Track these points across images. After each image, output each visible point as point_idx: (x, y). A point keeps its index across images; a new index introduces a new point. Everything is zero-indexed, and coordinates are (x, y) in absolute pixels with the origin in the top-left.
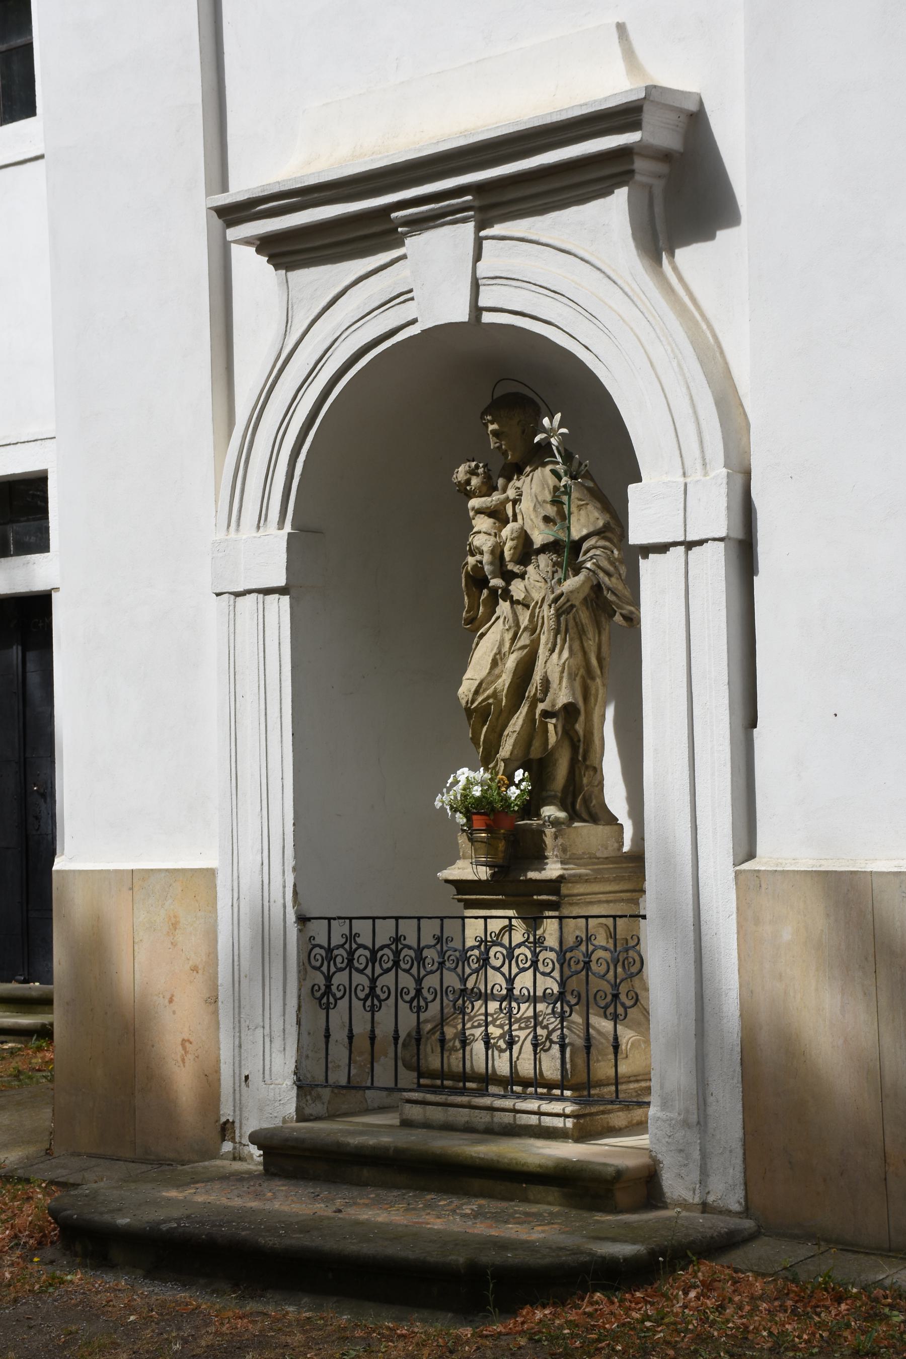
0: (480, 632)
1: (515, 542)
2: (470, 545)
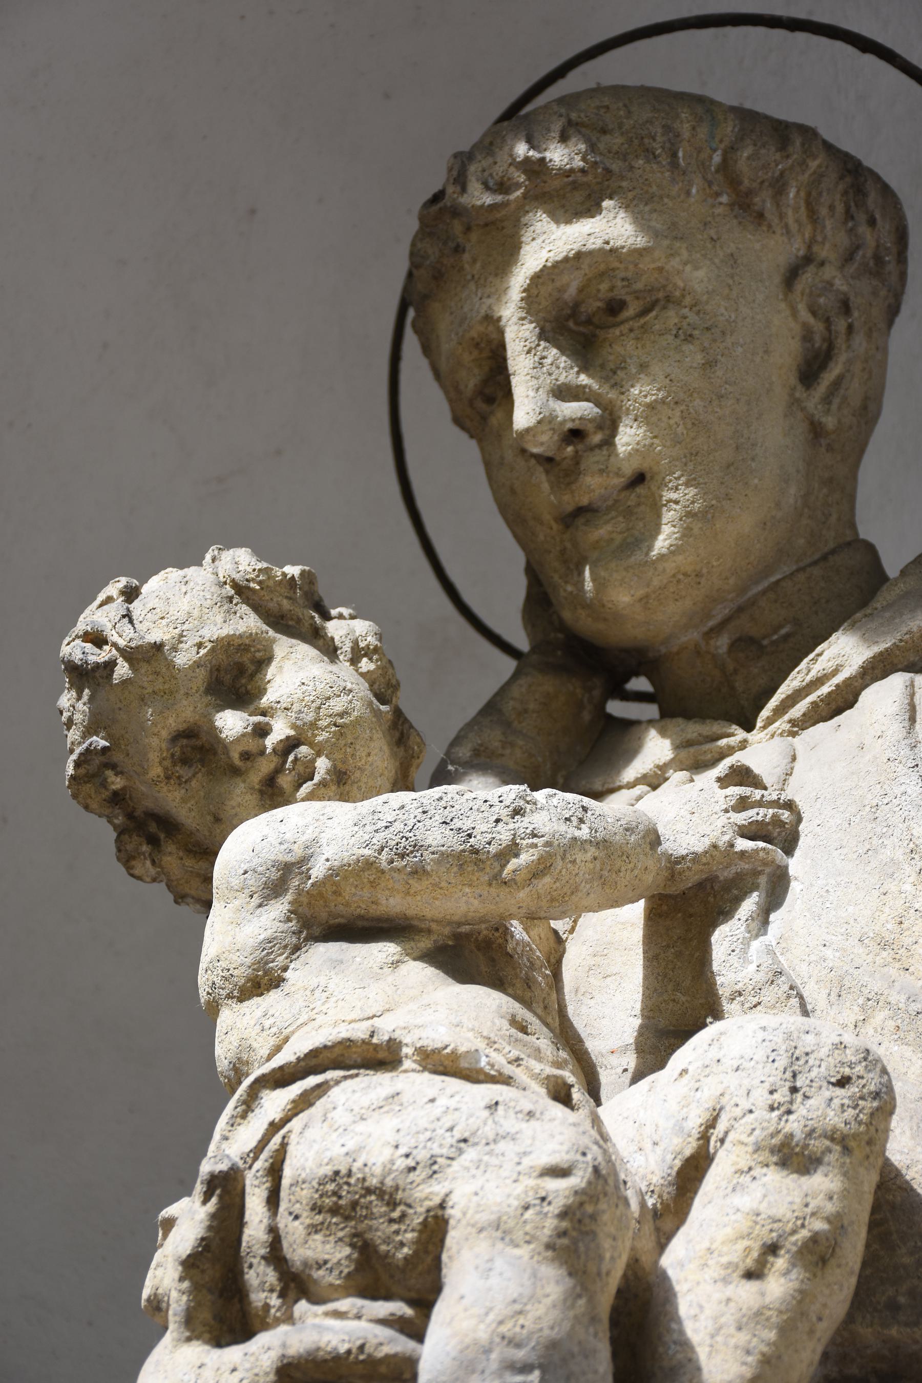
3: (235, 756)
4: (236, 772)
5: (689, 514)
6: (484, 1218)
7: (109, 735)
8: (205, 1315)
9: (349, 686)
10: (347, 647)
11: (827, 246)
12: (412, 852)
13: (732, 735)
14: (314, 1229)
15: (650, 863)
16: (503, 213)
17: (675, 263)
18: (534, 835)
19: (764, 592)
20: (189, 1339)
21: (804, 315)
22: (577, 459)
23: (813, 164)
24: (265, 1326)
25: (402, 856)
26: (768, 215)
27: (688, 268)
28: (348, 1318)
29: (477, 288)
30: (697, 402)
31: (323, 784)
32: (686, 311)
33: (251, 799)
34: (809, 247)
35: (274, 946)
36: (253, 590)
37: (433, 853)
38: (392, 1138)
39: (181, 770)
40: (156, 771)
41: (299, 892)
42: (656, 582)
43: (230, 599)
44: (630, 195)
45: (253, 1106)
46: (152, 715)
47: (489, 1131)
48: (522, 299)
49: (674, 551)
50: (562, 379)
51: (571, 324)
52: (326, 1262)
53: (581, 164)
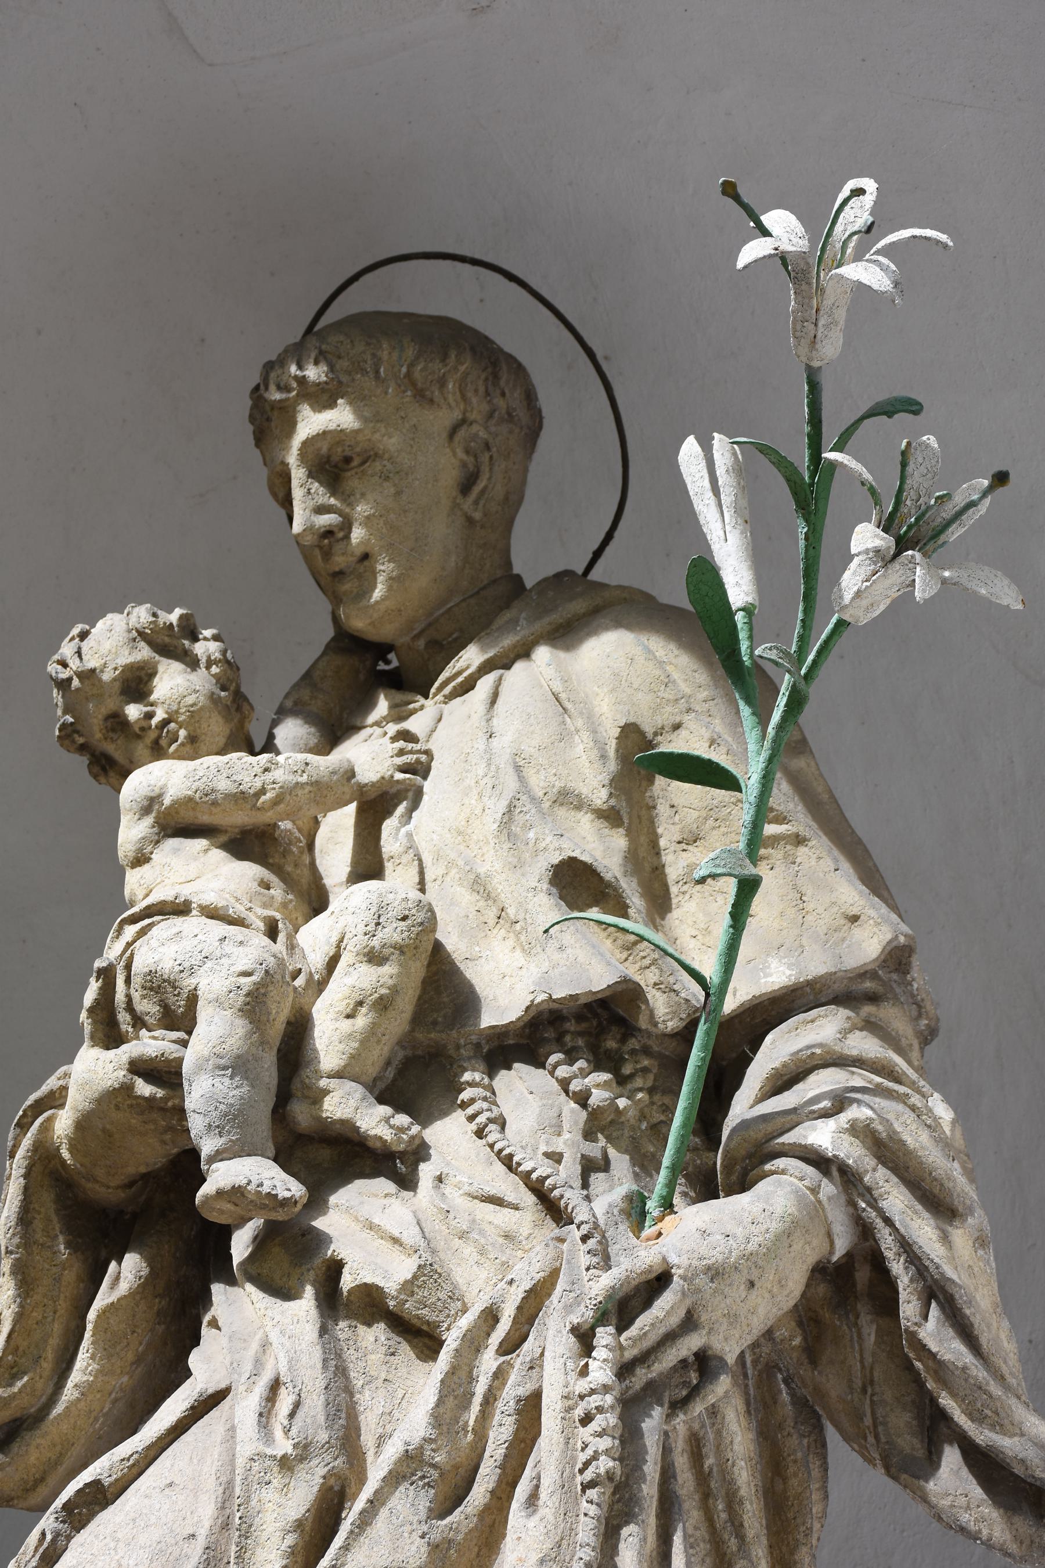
0: (85, 1477)
1: (388, 971)
2: (107, 974)
3: (137, 730)
4: (139, 737)
5: (391, 578)
6: (211, 996)
8: (100, 1035)
9: (198, 688)
10: (203, 660)
11: (475, 412)
13: (416, 702)
14: (143, 997)
15: (346, 789)
17: (377, 436)
18: (274, 783)
19: (443, 614)
20: (93, 1046)
21: (461, 454)
22: (330, 546)
23: (462, 368)
24: (128, 1041)
25: (206, 795)
26: (436, 400)
27: (385, 438)
30: (392, 516)
31: (182, 744)
32: (385, 462)
33: (146, 752)
34: (464, 414)
36: (147, 634)
38: (174, 956)
39: (111, 734)
40: (98, 735)
41: (159, 812)
42: (375, 616)
43: (134, 640)
44: (353, 396)
47: (218, 953)
49: (384, 599)
50: (320, 502)
51: (327, 467)
53: (325, 379)
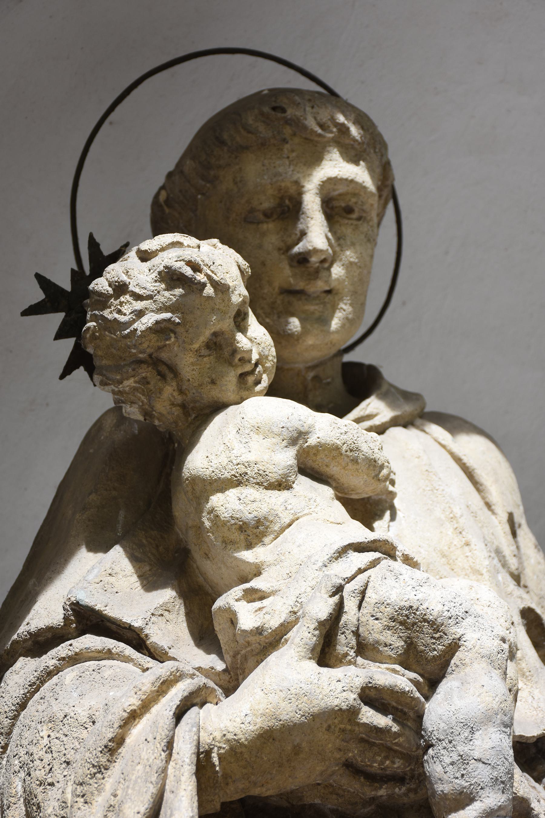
5: (347, 318)
6: (484, 652)
7: (183, 317)
12: (355, 451)
14: (389, 628)
16: (320, 139)
25: (351, 451)
28: (399, 674)
29: (290, 164)
35: (292, 470)
37: (363, 455)
41: (301, 447)
45: (342, 556)
46: (215, 320)
48: (319, 185)
52: (390, 645)
